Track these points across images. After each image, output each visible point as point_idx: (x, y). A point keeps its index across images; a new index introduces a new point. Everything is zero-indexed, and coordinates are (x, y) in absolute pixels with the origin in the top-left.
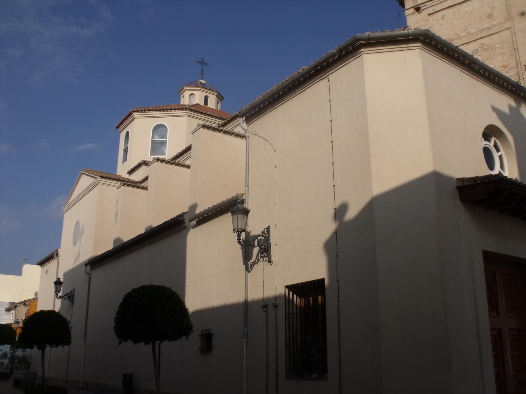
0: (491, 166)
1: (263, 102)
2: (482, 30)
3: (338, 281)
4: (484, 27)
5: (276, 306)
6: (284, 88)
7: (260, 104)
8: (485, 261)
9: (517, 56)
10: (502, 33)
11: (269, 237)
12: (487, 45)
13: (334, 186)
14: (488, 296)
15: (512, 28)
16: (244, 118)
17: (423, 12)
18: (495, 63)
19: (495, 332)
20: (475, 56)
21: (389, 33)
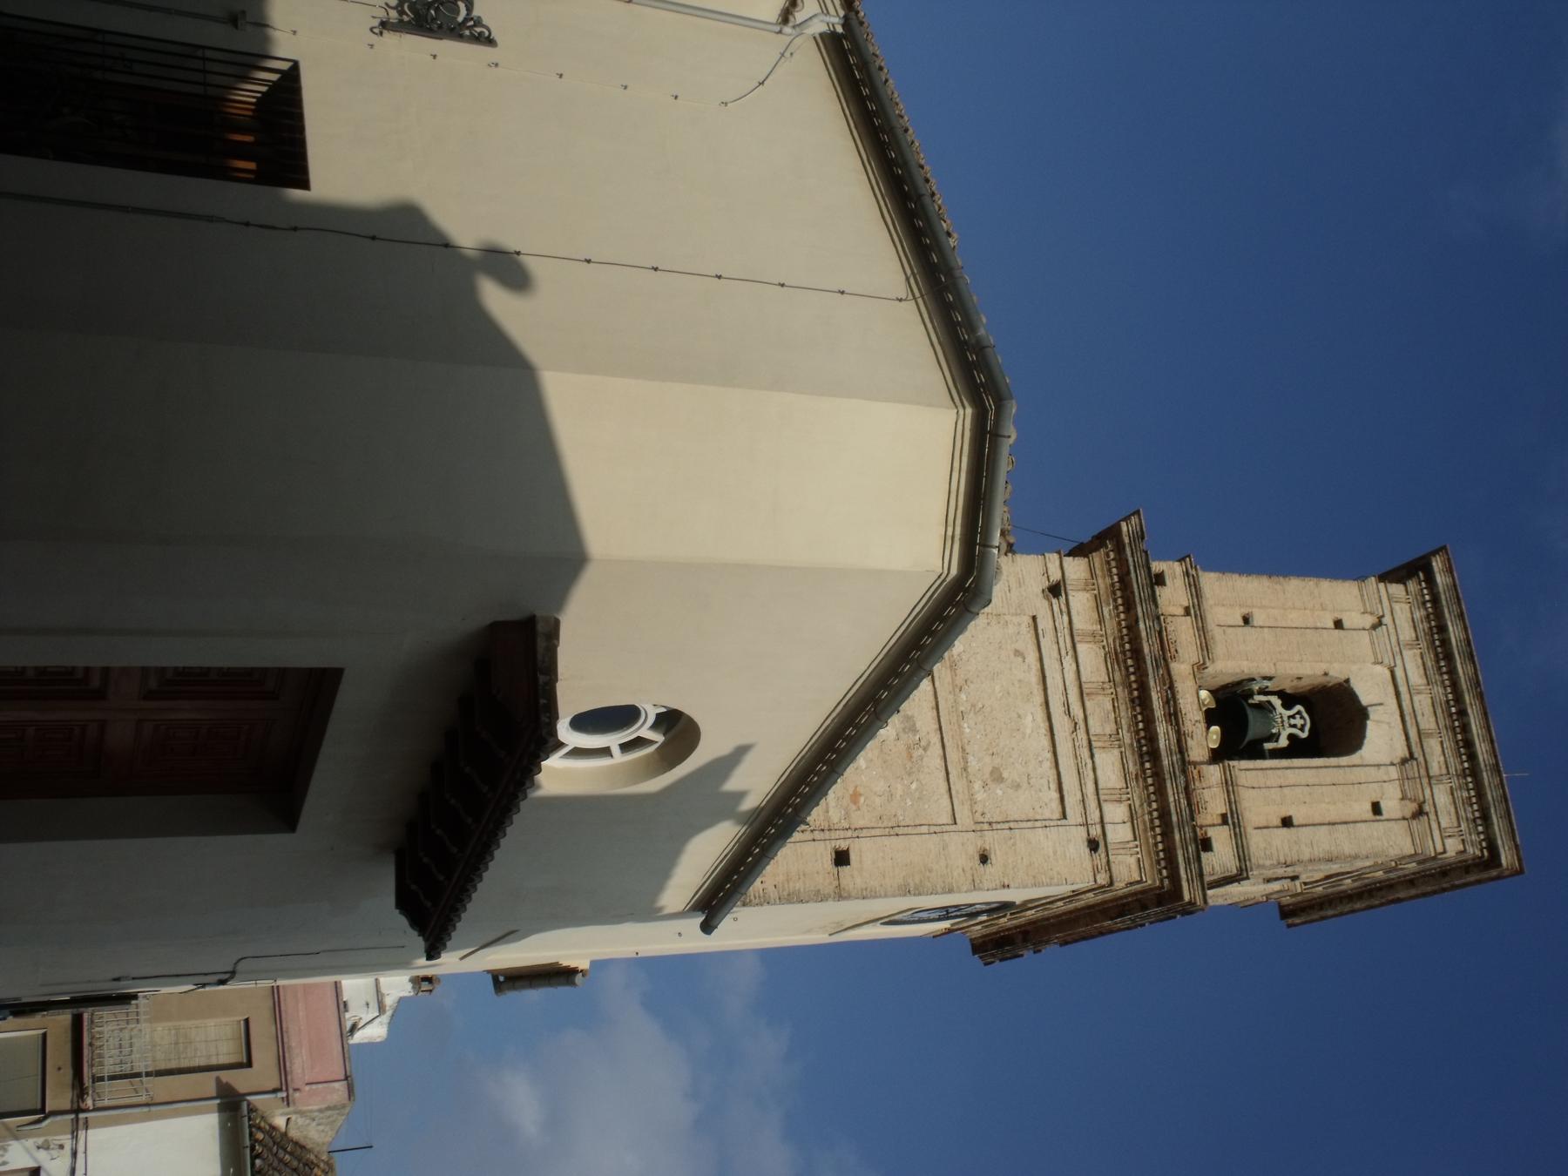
0: (584, 722)
1: (875, 96)
2: (964, 750)
3: (295, 229)
4: (970, 758)
5: (234, 20)
6: (905, 165)
7: (873, 88)
8: (311, 671)
9: (878, 832)
10: (946, 801)
11: (460, 37)
13: (589, 261)
14: (205, 672)
16: (840, 30)
17: (1046, 603)
18: (866, 770)
19: (96, 683)
20: (895, 720)
21: (1001, 493)
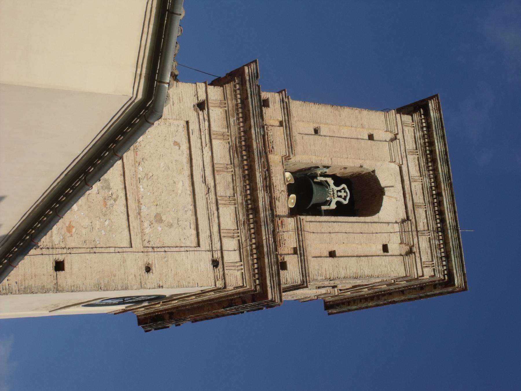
2: (139, 202)
4: (143, 207)
9: (83, 250)
12: (112, 205)
15: (130, 250)
17: (195, 114)
18: (79, 213)
20: (96, 187)
